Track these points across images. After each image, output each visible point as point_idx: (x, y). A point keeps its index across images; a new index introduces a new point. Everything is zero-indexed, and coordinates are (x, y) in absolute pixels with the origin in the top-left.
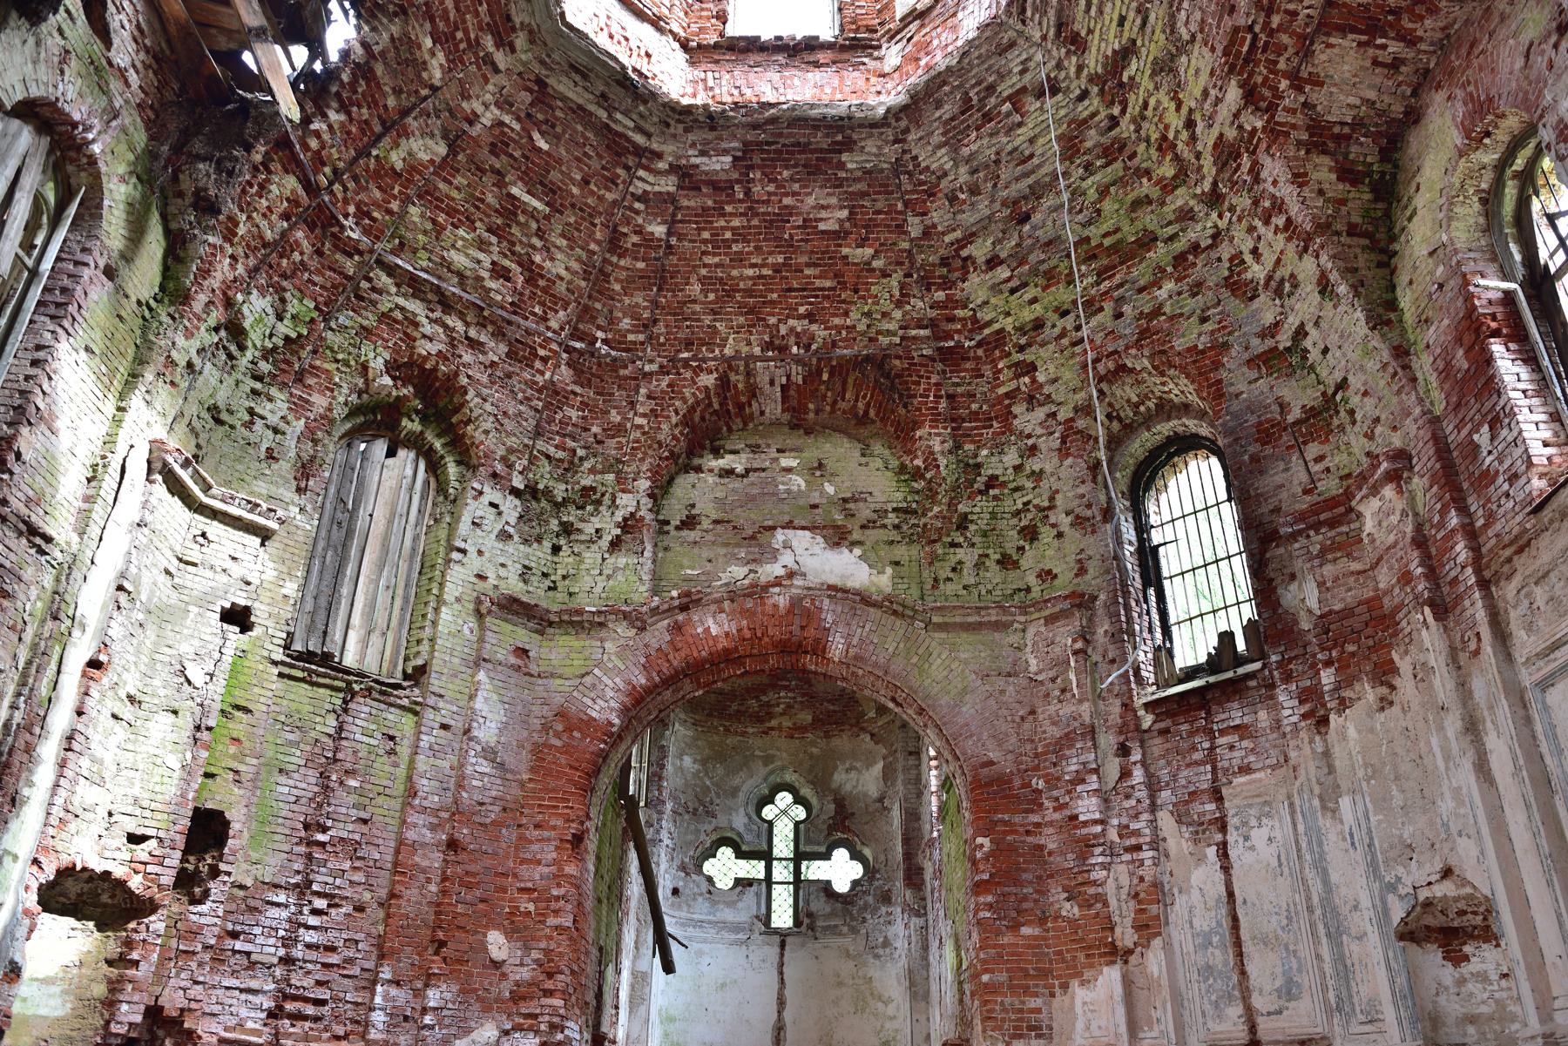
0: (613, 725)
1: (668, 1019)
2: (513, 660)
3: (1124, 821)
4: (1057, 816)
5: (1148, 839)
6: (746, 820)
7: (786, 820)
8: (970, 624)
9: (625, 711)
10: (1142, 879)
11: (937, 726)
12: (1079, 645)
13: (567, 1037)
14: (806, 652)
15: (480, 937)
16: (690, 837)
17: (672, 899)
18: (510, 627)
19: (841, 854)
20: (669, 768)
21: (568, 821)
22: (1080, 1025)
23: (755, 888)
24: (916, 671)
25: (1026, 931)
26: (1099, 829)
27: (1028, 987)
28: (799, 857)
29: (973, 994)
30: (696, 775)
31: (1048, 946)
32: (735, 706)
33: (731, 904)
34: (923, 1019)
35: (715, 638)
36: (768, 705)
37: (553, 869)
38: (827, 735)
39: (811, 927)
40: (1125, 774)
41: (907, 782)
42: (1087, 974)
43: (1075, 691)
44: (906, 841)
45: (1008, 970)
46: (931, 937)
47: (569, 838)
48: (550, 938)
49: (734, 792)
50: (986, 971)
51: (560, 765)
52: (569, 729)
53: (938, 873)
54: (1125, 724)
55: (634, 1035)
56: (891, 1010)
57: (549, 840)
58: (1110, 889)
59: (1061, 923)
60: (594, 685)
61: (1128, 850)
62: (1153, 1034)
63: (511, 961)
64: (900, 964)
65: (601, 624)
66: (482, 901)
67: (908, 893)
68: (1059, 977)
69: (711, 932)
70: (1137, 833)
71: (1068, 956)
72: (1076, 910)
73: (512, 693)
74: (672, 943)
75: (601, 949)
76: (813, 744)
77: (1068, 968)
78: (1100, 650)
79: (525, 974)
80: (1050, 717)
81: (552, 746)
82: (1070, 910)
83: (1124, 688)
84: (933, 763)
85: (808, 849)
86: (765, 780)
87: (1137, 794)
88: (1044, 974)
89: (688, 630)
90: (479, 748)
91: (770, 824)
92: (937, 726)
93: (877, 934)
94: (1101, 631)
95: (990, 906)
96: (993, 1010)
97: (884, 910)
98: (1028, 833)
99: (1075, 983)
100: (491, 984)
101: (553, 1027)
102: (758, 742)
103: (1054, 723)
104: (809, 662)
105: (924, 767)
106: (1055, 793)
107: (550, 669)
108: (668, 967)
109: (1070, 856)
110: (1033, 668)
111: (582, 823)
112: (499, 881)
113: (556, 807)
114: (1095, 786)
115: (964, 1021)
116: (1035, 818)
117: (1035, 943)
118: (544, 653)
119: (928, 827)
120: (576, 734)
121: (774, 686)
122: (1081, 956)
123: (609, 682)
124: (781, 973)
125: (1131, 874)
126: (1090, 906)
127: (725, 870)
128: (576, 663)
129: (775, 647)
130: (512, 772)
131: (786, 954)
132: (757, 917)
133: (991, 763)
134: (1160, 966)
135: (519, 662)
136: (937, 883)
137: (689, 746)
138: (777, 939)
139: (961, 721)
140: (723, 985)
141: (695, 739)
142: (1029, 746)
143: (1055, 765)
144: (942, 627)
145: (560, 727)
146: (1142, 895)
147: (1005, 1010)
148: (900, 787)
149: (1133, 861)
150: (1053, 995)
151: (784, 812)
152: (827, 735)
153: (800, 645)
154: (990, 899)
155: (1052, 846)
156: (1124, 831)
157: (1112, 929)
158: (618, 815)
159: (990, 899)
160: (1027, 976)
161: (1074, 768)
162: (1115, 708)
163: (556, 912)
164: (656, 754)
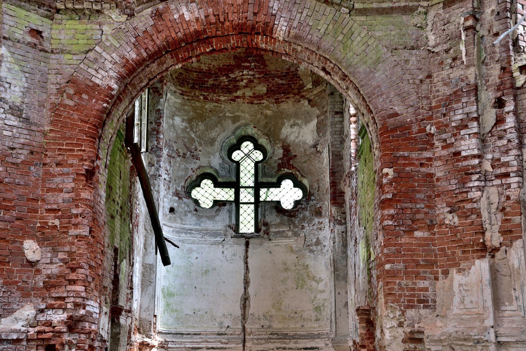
0: (112, 90)
1: (168, 294)
2: (29, 39)
3: (497, 155)
4: (445, 152)
5: (515, 169)
6: (220, 161)
7: (249, 161)
8: (384, 9)
9: (121, 79)
10: (508, 198)
11: (356, 88)
12: (470, 23)
13: (88, 312)
14: (258, 34)
15: (18, 245)
16: (181, 173)
17: (170, 215)
18: (24, 13)
19: (287, 184)
20: (164, 125)
21: (82, 160)
22: (457, 300)
23: (227, 207)
24: (341, 47)
25: (418, 234)
26: (476, 161)
27: (418, 273)
28: (257, 187)
29: (378, 277)
30: (184, 130)
31: (434, 245)
32: (211, 82)
33: (211, 218)
34: (343, 292)
35: (188, 23)
36: (235, 80)
37: (72, 195)
38: (277, 102)
39: (267, 233)
40: (500, 120)
41: (333, 134)
42: (463, 265)
43: (464, 59)
44: (333, 173)
45: (404, 262)
46: (349, 238)
47: (84, 172)
48: (73, 244)
49: (212, 142)
50: (388, 262)
51: (74, 120)
52: (78, 93)
53: (355, 196)
54: (502, 83)
55: (145, 306)
56: (321, 286)
57: (68, 174)
58: (483, 204)
59: (444, 229)
60: (96, 60)
61: (497, 177)
62: (513, 308)
63: (43, 261)
64: (327, 256)
65: (98, 11)
66: (18, 219)
67: (334, 209)
68: (441, 266)
69: (198, 237)
70: (507, 164)
71: (449, 252)
72: (456, 219)
73: (31, 65)
74: (168, 244)
75: (116, 250)
76: (267, 107)
77: (448, 260)
78: (487, 26)
79: (54, 269)
80: (443, 80)
81: (65, 106)
82: (452, 219)
83: (504, 55)
84: (353, 119)
85: (264, 180)
86: (234, 133)
87: (509, 136)
88: (431, 264)
89: (165, 16)
90: (7, 107)
91: (238, 163)
92: (356, 88)
93: (312, 236)
94: (488, 11)
95: (392, 217)
96: (393, 289)
97: (316, 220)
98: (422, 165)
99: (453, 271)
100: (28, 277)
101: (77, 305)
102: (229, 107)
103: (445, 84)
104: (260, 41)
105: (346, 122)
106: (444, 136)
107: (60, 47)
108: (166, 261)
109: (453, 181)
110: (432, 43)
111: (93, 162)
112: (31, 204)
113: (73, 150)
114: (475, 130)
115: (372, 295)
116: (427, 154)
117: (425, 243)
118: (55, 34)
119: (348, 164)
120: (85, 96)
121: (239, 67)
122: (459, 252)
123: (108, 57)
124: (246, 263)
125: (500, 194)
126: (467, 217)
127: (207, 195)
128: (80, 42)
129: (234, 29)
130: (36, 124)
131: (250, 250)
132: (229, 226)
133: (396, 115)
134: (520, 260)
135: (35, 41)
136: (353, 202)
137: (179, 110)
138: (243, 241)
139: (374, 83)
140: (207, 272)
141: (183, 105)
142: (425, 102)
143: (444, 115)
144: (363, 12)
145: (71, 91)
146: (508, 209)
147: (401, 289)
148: (328, 136)
149: (502, 185)
150: (437, 279)
151: (247, 155)
152: (277, 102)
153: (253, 28)
154: (392, 211)
155: (439, 174)
156: (496, 163)
157: (483, 233)
158: (126, 158)
159: (392, 211)
160: (418, 265)
161: (459, 117)
162: (495, 71)
163: (76, 225)
164: (154, 116)
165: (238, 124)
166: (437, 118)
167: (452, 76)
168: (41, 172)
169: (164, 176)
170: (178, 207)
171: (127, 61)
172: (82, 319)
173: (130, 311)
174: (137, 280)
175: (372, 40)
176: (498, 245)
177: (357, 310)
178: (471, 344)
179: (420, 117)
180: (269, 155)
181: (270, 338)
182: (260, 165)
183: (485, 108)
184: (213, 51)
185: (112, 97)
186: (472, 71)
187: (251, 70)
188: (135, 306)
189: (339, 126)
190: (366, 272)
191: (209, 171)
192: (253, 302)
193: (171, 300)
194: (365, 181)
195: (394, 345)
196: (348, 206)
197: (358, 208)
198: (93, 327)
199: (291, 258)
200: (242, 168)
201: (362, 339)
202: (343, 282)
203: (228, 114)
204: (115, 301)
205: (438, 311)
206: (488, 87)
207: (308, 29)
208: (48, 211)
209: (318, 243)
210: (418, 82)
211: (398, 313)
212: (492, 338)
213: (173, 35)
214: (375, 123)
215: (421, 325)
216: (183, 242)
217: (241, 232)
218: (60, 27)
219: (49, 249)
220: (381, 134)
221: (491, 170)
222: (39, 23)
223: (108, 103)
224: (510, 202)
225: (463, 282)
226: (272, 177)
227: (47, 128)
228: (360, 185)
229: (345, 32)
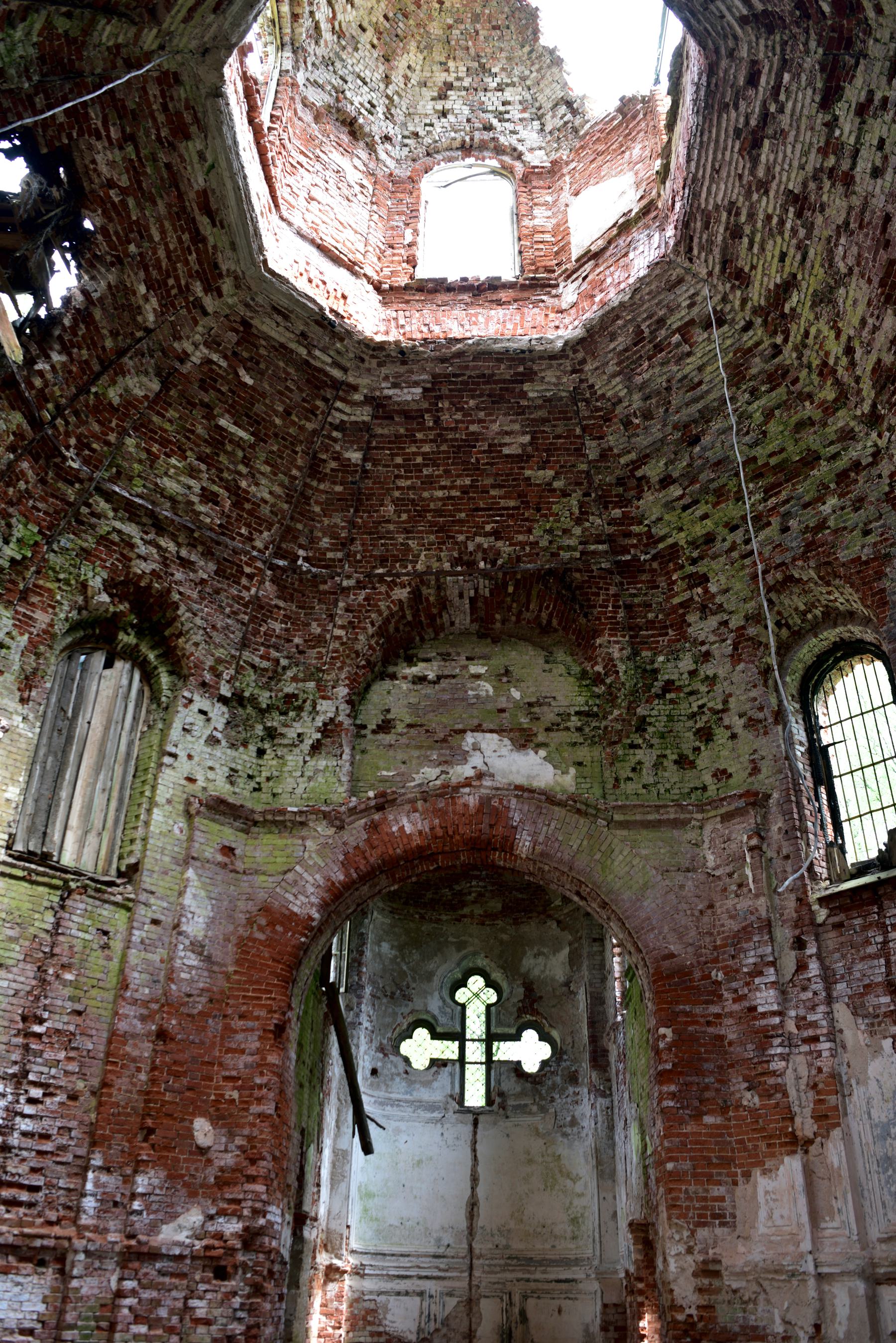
0: (313, 920)
1: (367, 1195)
3: (802, 1012)
4: (736, 1007)
5: (825, 1031)
6: (440, 1003)
8: (650, 822)
9: (324, 906)
10: (820, 1070)
11: (620, 919)
13: (269, 1222)
14: (495, 849)
15: (187, 1124)
16: (388, 1020)
17: (372, 1080)
19: (530, 1035)
20: (368, 954)
21: (270, 1011)
22: (762, 1214)
25: (709, 1119)
26: (777, 1020)
27: (711, 1175)
28: (490, 1039)
29: (658, 1181)
30: (393, 960)
31: (730, 1135)
32: (429, 895)
33: (427, 1084)
34: (609, 1197)
36: (461, 893)
38: (516, 922)
39: (503, 1106)
40: (802, 966)
43: (752, 886)
44: (592, 1024)
45: (692, 1159)
46: (616, 1117)
48: (253, 1125)
49: (429, 976)
51: (263, 958)
52: (271, 924)
53: (623, 1057)
54: (800, 918)
55: (335, 1211)
56: (579, 1187)
57: (252, 1030)
58: (789, 1079)
60: (296, 882)
61: (806, 1041)
62: (835, 1224)
63: (216, 1147)
64: (587, 1143)
68: (741, 1166)
69: (408, 1111)
70: (814, 1025)
72: (756, 1099)
75: (302, 1132)
76: (503, 930)
77: (750, 1157)
79: (229, 1160)
80: (728, 910)
81: (255, 940)
82: (751, 1099)
88: (726, 1162)
92: (620, 919)
93: (565, 1112)
95: (673, 1096)
97: (571, 1090)
98: (709, 1023)
99: (757, 1172)
100: (196, 1169)
103: (732, 917)
104: (497, 857)
105: (608, 954)
106: (734, 985)
107: (254, 866)
108: (367, 1149)
109: (750, 1047)
110: (711, 863)
111: (284, 1014)
113: (260, 998)
114: (773, 979)
115: (649, 1205)
116: (715, 1009)
117: (717, 1132)
119: (612, 1010)
120: (279, 928)
122: (763, 1146)
123: (310, 879)
124: (474, 1150)
125: (810, 1065)
126: (770, 1096)
128: (278, 860)
132: (451, 1096)
133: (672, 956)
134: (840, 1157)
135: (226, 860)
136: (621, 1066)
138: (470, 1117)
139: (643, 915)
140: (420, 1162)
142: (708, 939)
143: (733, 957)
145: (263, 922)
146: (821, 1086)
148: (585, 972)
149: (811, 1052)
150: (735, 1183)
153: (489, 842)
154: (673, 1088)
155: (732, 1036)
157: (792, 1119)
159: (673, 1088)
161: (751, 961)
163: (259, 1100)
165: (464, 952)
166: (724, 960)
167: (738, 907)
168: (220, 1027)
169: (366, 1024)
170: (383, 1067)
171: (333, 883)
172: (261, 1232)
173: (315, 1219)
174: (325, 1173)
175: (637, 860)
176: (811, 1136)
177: (631, 1225)
178: (784, 1277)
179: (703, 959)
180: (505, 995)
181: (507, 1265)
182: (493, 1009)
183: (781, 950)
184: (439, 868)
185: (311, 929)
186: (762, 902)
187: (483, 880)
188: (322, 1211)
189: (598, 958)
190: (641, 1170)
191: (425, 1017)
192: (483, 1209)
193: (371, 1203)
194: (636, 1040)
195: (681, 1281)
196: (614, 1071)
197: (628, 1076)
198: (274, 1244)
199: (537, 1145)
200: (468, 1012)
201: (638, 1269)
202: (610, 1182)
203: (451, 939)
204: (299, 1204)
205: (739, 1227)
206: (784, 922)
207: (557, 845)
208: (227, 1078)
209: (574, 1122)
210: (697, 913)
211: (686, 1234)
212: (810, 1268)
213: (391, 852)
214: (646, 965)
215: (717, 1250)
216: (388, 1117)
217: (467, 1104)
218: (256, 842)
219: (224, 1131)
220: (655, 982)
221: (795, 1031)
222: (232, 838)
223: (306, 936)
224: (822, 1076)
225: (769, 1188)
226: (509, 1026)
227: (231, 969)
228: (629, 1043)
229: (603, 848)
